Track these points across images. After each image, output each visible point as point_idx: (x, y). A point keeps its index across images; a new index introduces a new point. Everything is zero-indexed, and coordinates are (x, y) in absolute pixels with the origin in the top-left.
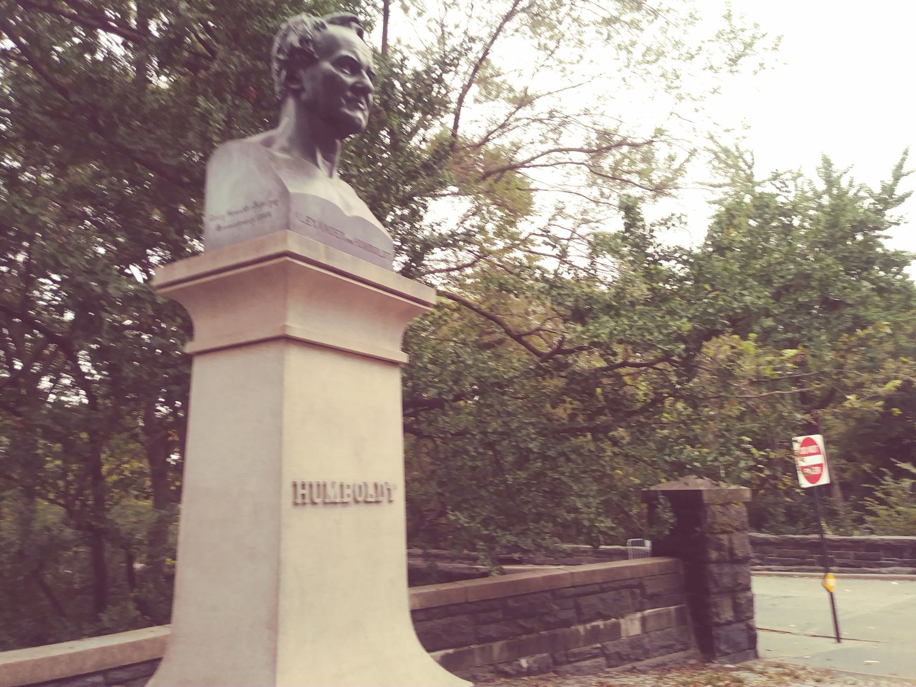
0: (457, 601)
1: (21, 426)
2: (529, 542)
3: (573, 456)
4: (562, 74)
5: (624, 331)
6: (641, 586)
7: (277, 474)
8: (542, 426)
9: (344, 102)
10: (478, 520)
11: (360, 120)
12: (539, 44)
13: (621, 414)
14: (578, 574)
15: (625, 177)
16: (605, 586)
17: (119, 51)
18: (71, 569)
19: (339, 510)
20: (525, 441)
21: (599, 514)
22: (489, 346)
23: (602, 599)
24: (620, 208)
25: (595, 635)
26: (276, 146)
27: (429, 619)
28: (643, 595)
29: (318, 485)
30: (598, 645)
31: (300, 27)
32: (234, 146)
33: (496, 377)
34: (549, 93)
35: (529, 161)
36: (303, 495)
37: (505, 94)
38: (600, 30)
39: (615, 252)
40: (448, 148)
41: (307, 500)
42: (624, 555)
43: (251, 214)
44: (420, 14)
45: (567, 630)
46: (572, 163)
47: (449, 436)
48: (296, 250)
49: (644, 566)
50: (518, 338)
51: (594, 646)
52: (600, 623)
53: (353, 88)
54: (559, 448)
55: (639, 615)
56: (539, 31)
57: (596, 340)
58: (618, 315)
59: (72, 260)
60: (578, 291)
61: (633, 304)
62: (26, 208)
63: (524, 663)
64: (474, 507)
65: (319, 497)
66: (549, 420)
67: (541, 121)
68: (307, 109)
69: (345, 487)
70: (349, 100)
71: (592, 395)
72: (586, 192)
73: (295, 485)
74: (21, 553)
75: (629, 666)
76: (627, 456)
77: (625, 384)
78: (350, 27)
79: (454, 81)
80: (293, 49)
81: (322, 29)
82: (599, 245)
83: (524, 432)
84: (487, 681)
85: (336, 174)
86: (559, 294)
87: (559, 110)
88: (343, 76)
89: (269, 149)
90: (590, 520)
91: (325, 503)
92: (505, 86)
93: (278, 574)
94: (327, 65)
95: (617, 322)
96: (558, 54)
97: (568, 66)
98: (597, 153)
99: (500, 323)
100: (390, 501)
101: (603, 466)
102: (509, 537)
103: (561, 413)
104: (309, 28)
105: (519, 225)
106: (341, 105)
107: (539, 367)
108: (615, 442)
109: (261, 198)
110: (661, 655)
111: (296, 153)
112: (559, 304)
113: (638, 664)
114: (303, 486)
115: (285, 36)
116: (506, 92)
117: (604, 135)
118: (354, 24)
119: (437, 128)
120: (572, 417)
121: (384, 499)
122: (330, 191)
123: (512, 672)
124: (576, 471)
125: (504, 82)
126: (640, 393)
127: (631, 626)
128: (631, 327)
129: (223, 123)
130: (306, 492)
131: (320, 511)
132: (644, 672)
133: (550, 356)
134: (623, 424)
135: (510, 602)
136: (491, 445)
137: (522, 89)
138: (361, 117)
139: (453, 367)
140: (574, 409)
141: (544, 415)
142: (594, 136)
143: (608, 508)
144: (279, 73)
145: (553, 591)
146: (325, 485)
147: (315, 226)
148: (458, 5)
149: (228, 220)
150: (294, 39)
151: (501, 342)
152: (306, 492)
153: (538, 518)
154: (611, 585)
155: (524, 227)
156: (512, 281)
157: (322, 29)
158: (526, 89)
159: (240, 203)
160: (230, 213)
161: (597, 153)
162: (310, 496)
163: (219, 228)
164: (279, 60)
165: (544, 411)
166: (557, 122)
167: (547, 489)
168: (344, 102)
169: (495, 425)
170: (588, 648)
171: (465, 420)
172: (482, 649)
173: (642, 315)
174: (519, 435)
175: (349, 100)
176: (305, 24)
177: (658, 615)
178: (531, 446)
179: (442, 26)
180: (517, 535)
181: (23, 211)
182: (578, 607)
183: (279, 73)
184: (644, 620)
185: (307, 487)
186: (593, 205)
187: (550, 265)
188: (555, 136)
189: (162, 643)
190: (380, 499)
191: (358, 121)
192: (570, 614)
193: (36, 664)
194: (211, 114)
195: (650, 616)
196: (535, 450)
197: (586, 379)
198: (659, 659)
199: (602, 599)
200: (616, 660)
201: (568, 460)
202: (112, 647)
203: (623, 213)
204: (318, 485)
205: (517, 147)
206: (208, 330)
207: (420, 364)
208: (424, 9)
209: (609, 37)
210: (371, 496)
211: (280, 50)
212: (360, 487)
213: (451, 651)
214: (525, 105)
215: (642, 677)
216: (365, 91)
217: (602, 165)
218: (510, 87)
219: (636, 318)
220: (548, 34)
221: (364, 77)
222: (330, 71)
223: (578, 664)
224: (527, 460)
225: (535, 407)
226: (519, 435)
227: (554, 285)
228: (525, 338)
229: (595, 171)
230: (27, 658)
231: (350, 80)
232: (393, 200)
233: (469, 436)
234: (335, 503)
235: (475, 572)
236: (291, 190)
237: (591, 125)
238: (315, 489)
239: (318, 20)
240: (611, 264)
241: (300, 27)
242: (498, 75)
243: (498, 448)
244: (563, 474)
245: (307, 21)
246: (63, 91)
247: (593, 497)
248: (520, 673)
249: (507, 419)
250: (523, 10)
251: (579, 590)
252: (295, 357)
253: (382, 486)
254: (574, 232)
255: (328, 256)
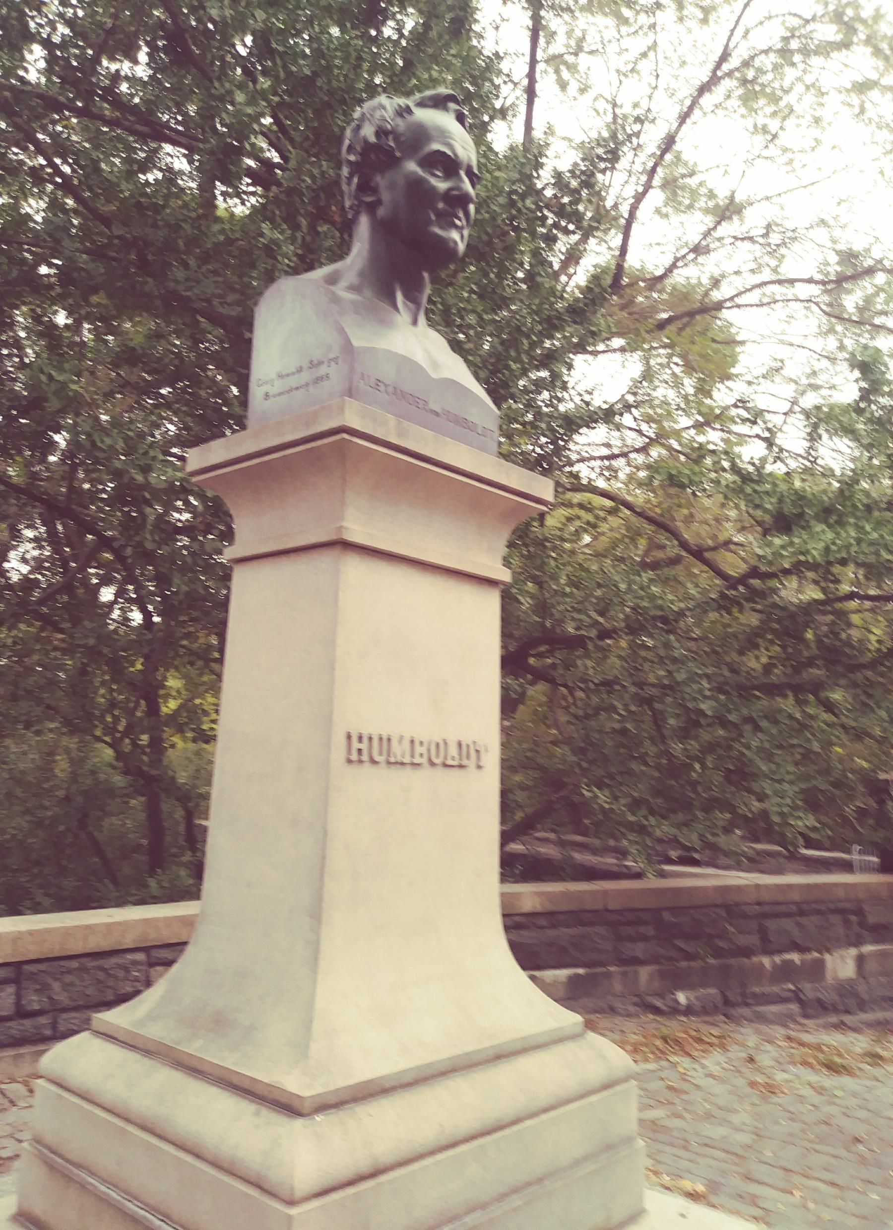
0: (595, 907)
1: (64, 645)
2: (695, 837)
3: (764, 724)
4: (789, 168)
5: (848, 547)
6: (860, 913)
7: (328, 721)
8: (721, 679)
9: (433, 217)
10: (623, 801)
11: (456, 243)
12: (755, 125)
13: (840, 669)
14: (766, 887)
15: (877, 321)
16: (806, 907)
17: (181, 164)
18: (127, 821)
19: (408, 771)
20: (695, 699)
21: (795, 808)
22: (655, 566)
23: (799, 925)
24: (853, 366)
25: (786, 972)
26: (343, 284)
27: (553, 926)
28: (862, 924)
29: (381, 739)
30: (792, 987)
31: (378, 114)
32: (287, 285)
33: (660, 608)
34: (767, 198)
35: (731, 299)
36: (360, 750)
37: (702, 203)
38: (849, 100)
39: (849, 431)
40: (613, 282)
41: (365, 757)
42: (847, 867)
43: (305, 377)
44: (582, 91)
45: (746, 960)
46: (797, 300)
47: (592, 686)
48: (355, 423)
49: (867, 886)
50: (698, 554)
51: (784, 987)
52: (795, 957)
53: (447, 196)
54: (745, 712)
55: (853, 951)
56: (755, 106)
57: (802, 558)
58: (840, 523)
59: (108, 441)
60: (783, 487)
61: (869, 508)
62: (53, 373)
63: (682, 997)
64: (621, 784)
65: (381, 754)
66: (733, 671)
67: (751, 239)
68: (384, 230)
69: (417, 743)
70: (440, 215)
71: (801, 640)
72: (818, 344)
73: (349, 737)
74: (67, 799)
75: (833, 1019)
76: (843, 726)
77: (849, 625)
78: (446, 109)
79: (617, 186)
80: (368, 148)
81: (405, 114)
82: (820, 420)
83: (695, 687)
84: (629, 1015)
85: (422, 319)
86: (755, 491)
87: (779, 221)
88: (433, 181)
89: (332, 288)
90: (781, 814)
91: (389, 763)
92: (703, 190)
93: (323, 849)
94: (412, 166)
95: (838, 534)
96: (784, 139)
97: (797, 156)
98: (839, 284)
99: (674, 534)
100: (479, 767)
101: (808, 740)
102: (665, 828)
103: (754, 662)
104: (389, 114)
105: (715, 394)
106: (429, 222)
107: (723, 596)
108: (830, 707)
109: (318, 355)
110: (884, 1009)
111: (368, 292)
112: (757, 506)
113: (847, 1019)
114: (360, 739)
115: (359, 127)
116: (704, 199)
117: (849, 257)
118: (452, 105)
119: (598, 254)
120: (768, 669)
121: (472, 764)
122: (416, 344)
123: (664, 1008)
124: (767, 745)
125: (701, 184)
126: (873, 638)
127: (842, 965)
128: (859, 541)
129: (295, 259)
130: (364, 746)
131: (383, 771)
132: (855, 1030)
133: (743, 580)
134: (843, 682)
135: (666, 916)
136: (648, 701)
137: (729, 194)
138: (458, 238)
139: (598, 593)
140: (770, 657)
141: (727, 664)
142: (834, 258)
143: (812, 802)
144: (350, 179)
145: (730, 905)
146: (389, 740)
147: (386, 392)
148: (638, 73)
149: (279, 386)
150: (368, 132)
151: (675, 561)
152: (364, 746)
153: (709, 806)
154: (815, 906)
155: (723, 396)
156: (687, 472)
157: (405, 114)
158: (733, 192)
159: (292, 363)
160: (280, 376)
161: (839, 284)
162: (366, 751)
163: (267, 395)
164: (349, 162)
165: (728, 659)
166: (774, 240)
167: (732, 768)
168: (433, 217)
169: (656, 674)
170: (775, 989)
171: (614, 665)
172: (624, 974)
173: (879, 524)
174: (688, 690)
175: (440, 215)
176: (384, 108)
177: (883, 954)
178: (703, 706)
179: (615, 105)
180: (678, 826)
181: (51, 378)
182: (763, 933)
183: (350, 179)
184: (860, 960)
185: (365, 740)
186: (825, 363)
187: (751, 452)
188: (773, 263)
189: (189, 922)
190: (465, 762)
191: (452, 244)
192: (753, 940)
193: (67, 932)
194: (279, 247)
195: (872, 954)
196: (709, 713)
197: (792, 616)
198: (880, 1015)
199: (799, 925)
200: (815, 1008)
201: (757, 728)
202: (157, 920)
203: (857, 374)
204: (381, 739)
205: (716, 283)
206: (251, 530)
207: (554, 587)
208: (589, 83)
209: (862, 110)
210: (453, 758)
211: (350, 149)
212: (438, 745)
213: (581, 971)
214: (730, 218)
215: (852, 1036)
216: (462, 200)
217: (845, 303)
218: (711, 191)
219: (868, 528)
220: (769, 110)
221: (461, 180)
222: (415, 173)
223: (758, 1009)
224: (697, 724)
225: (715, 652)
226: (688, 690)
227: (748, 482)
228: (707, 555)
229: (836, 314)
230: (58, 925)
231: (443, 186)
232: (525, 359)
233: (617, 687)
234: (402, 764)
235: (625, 870)
236: (356, 343)
237: (830, 245)
238: (375, 743)
239: (402, 101)
240: (849, 451)
241: (378, 114)
242: (691, 174)
243: (657, 706)
244: (748, 747)
245: (386, 105)
246: (107, 221)
247: (791, 783)
248: (675, 1011)
249: (671, 667)
250: (730, 74)
251: (767, 909)
252: (354, 569)
253: (468, 746)
254: (794, 403)
255: (401, 433)
